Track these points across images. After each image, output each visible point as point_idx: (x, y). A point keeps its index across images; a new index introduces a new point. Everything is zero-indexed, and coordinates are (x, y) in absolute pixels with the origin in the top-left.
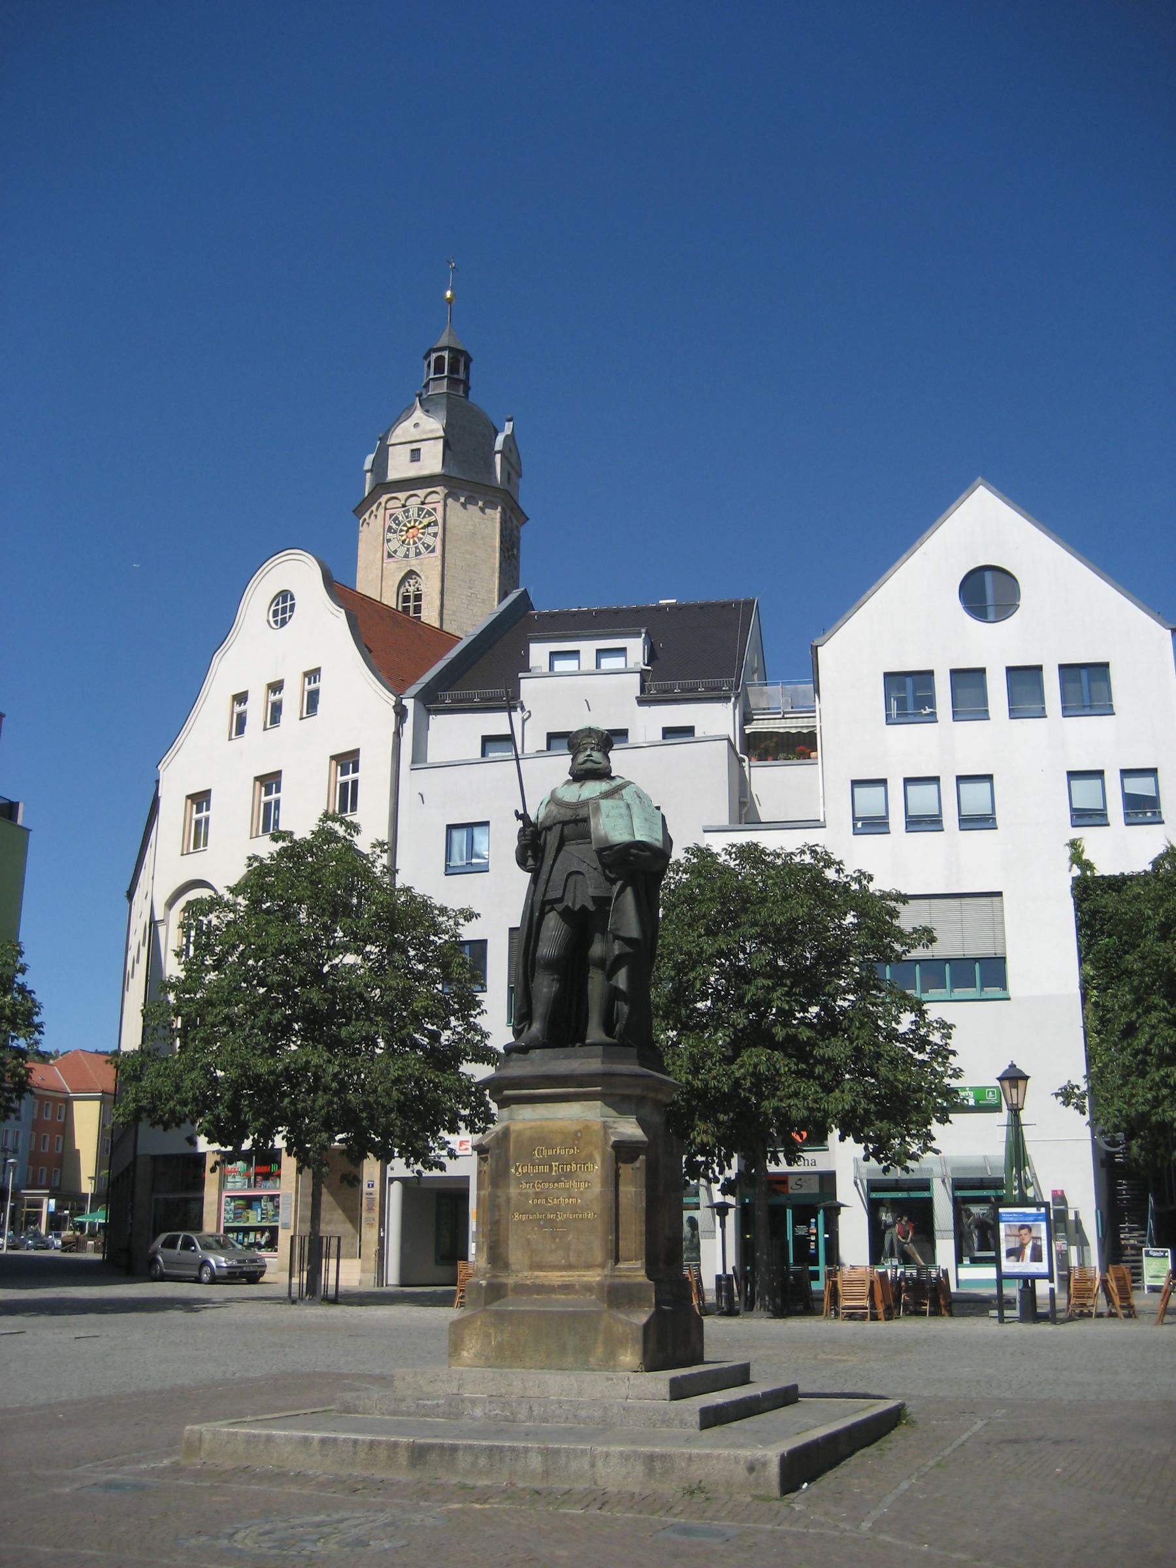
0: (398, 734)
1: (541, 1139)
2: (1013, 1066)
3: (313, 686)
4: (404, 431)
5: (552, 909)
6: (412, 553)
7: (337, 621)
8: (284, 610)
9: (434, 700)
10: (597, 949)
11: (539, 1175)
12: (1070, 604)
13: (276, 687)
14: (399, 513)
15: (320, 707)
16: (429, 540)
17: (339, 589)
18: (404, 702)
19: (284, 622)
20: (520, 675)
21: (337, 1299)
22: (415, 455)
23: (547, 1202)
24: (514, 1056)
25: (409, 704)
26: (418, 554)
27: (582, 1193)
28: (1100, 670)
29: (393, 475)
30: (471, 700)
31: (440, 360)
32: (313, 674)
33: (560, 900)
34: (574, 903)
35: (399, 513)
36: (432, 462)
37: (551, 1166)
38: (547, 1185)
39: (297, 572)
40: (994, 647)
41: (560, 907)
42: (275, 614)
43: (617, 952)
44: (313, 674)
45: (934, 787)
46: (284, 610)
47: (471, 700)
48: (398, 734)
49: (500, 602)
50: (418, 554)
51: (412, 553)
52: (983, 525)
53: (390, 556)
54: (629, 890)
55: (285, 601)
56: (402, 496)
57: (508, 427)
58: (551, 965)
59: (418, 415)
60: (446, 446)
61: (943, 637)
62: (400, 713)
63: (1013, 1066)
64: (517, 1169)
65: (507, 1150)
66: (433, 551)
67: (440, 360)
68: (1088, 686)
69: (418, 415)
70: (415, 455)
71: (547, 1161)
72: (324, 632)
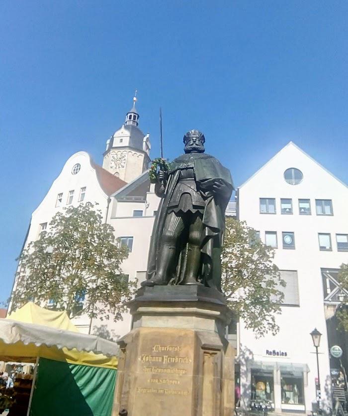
0: (108, 207)
1: (158, 339)
2: (316, 330)
3: (83, 192)
4: (118, 134)
5: (173, 211)
6: (118, 167)
7: (93, 173)
8: (77, 170)
9: (120, 199)
10: (196, 235)
11: (155, 364)
12: (318, 180)
13: (72, 192)
14: (115, 156)
15: (80, 173)
16: (123, 164)
17: (96, 164)
18: (111, 198)
19: (77, 173)
20: (147, 192)
21: (283, 237)
22: (121, 140)
23: (159, 381)
24: (147, 288)
25: (112, 198)
26: (119, 168)
27: (180, 377)
28: (328, 202)
29: (114, 146)
30: (131, 199)
31: (131, 116)
32: (84, 188)
33: (177, 206)
34: (184, 208)
35: (115, 156)
36: (126, 142)
37: (163, 358)
38: (160, 370)
39: (82, 158)
40: (295, 192)
41: (176, 210)
42: (74, 170)
43: (207, 235)
44: (84, 188)
45: (275, 236)
46: (77, 170)
47: (131, 199)
48: (108, 207)
49: (143, 172)
50: (119, 168)
51: (118, 167)
52: (291, 155)
53: (111, 168)
54: (213, 201)
55: (78, 166)
56: (116, 151)
57: (148, 136)
58: (170, 240)
59: (123, 129)
60: (130, 137)
61: (280, 189)
62: (109, 201)
63: (316, 330)
64: (142, 359)
65: (137, 346)
66: (124, 167)
67: (131, 116)
68: (325, 204)
69: (123, 129)
70: (121, 140)
71: (161, 354)
72: (89, 175)
